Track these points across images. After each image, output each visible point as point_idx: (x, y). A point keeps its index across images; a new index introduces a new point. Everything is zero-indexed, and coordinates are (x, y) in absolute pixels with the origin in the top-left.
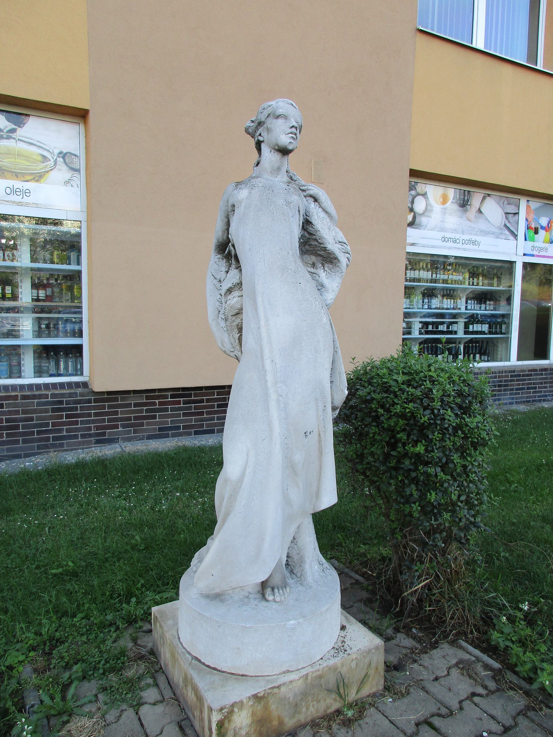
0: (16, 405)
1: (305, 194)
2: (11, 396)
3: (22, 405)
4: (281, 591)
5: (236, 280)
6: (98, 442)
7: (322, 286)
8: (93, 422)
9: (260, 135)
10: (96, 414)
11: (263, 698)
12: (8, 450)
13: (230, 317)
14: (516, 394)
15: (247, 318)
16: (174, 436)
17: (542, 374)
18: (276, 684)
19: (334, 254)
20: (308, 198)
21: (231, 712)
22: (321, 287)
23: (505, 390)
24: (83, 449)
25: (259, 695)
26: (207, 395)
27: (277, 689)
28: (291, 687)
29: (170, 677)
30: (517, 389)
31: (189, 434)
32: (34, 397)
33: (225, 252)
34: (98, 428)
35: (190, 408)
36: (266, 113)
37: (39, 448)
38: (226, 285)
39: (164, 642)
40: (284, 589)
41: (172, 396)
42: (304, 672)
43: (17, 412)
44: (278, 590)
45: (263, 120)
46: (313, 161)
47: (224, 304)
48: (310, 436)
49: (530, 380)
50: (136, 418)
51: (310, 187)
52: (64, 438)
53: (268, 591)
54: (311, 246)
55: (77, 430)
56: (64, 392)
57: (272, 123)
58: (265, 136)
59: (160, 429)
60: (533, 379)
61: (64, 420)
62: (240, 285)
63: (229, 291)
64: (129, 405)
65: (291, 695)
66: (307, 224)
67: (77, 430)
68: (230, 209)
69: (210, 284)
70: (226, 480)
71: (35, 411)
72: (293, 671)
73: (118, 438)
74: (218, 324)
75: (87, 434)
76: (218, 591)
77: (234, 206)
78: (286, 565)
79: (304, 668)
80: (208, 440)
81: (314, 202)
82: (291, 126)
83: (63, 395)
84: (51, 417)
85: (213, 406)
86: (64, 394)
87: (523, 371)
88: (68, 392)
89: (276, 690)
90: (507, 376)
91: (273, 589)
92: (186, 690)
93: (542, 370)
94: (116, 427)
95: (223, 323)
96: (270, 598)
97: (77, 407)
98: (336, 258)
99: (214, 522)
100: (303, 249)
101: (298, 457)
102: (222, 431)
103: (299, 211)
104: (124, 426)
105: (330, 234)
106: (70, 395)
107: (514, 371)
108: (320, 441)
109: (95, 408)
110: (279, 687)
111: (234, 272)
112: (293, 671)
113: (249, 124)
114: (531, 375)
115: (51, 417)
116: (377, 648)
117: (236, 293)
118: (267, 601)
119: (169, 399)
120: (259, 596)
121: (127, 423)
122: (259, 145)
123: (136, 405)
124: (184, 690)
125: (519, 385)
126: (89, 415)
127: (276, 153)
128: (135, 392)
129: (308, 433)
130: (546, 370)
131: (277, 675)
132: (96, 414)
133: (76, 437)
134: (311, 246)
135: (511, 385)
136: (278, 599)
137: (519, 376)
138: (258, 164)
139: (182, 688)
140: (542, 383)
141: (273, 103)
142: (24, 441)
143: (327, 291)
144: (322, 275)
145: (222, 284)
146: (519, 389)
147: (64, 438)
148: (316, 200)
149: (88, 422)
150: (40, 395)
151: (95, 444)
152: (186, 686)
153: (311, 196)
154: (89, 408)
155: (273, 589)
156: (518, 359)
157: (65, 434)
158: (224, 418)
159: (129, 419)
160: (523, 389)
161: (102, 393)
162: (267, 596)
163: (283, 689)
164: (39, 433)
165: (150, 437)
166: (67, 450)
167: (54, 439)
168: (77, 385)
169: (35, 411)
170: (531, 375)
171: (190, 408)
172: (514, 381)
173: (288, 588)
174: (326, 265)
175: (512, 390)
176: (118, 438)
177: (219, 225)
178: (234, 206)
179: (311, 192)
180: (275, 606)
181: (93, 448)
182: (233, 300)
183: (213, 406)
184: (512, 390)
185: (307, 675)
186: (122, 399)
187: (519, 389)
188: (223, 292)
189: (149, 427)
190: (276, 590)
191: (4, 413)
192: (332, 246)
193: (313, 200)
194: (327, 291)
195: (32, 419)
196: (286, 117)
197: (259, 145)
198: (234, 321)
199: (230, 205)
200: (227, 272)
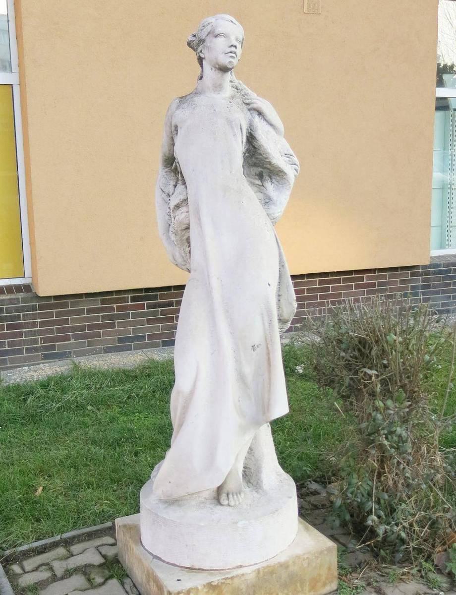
1: (249, 107)
4: (235, 496)
5: (182, 197)
6: (46, 357)
7: (270, 199)
8: (40, 333)
9: (201, 51)
10: (43, 324)
13: (180, 232)
15: (193, 233)
18: (229, 576)
19: (279, 168)
20: (252, 112)
24: (28, 366)
25: (213, 584)
27: (230, 580)
28: (243, 579)
29: (134, 580)
31: (156, 345)
33: (172, 165)
34: (45, 340)
35: (156, 313)
36: (205, 31)
38: (174, 201)
39: (128, 549)
40: (239, 495)
41: (134, 299)
42: (256, 567)
44: (233, 496)
45: (203, 38)
47: (173, 219)
48: (258, 349)
51: (254, 101)
53: (223, 497)
54: (258, 164)
55: (21, 343)
56: (4, 298)
57: (212, 42)
58: (206, 54)
59: (120, 340)
61: (5, 331)
62: (185, 201)
63: (177, 207)
64: (81, 312)
65: (243, 587)
66: (251, 139)
67: (21, 343)
68: (173, 128)
69: (158, 197)
70: (178, 392)
72: (246, 566)
73: (70, 352)
74: (169, 238)
77: (177, 127)
78: (243, 476)
79: (257, 564)
80: (158, 355)
81: (258, 114)
82: (230, 45)
86: (3, 300)
88: (8, 297)
89: (228, 581)
91: (228, 495)
92: (149, 585)
94: (67, 338)
95: (173, 238)
96: (226, 502)
97: (19, 316)
98: (282, 171)
100: (250, 161)
101: (248, 370)
102: (172, 343)
103: (241, 129)
104: (76, 337)
105: (275, 147)
106: (11, 301)
109: (41, 316)
110: (232, 578)
111: (180, 187)
112: (246, 566)
113: (190, 38)
116: (329, 550)
118: (222, 505)
119: (130, 303)
120: (215, 501)
121: (80, 333)
122: (200, 60)
123: (90, 311)
124: (148, 586)
126: (34, 325)
127: (217, 71)
128: (88, 295)
129: (256, 346)
131: (231, 569)
132: (43, 324)
133: (20, 351)
134: (258, 164)
136: (232, 503)
139: (146, 585)
141: (211, 20)
144: (270, 187)
145: (171, 198)
148: (260, 113)
149: (34, 333)
151: (43, 359)
152: (148, 582)
153: (255, 109)
154: (34, 316)
157: (7, 348)
159: (82, 328)
161: (49, 298)
162: (222, 501)
163: (236, 581)
165: (108, 350)
166: (11, 368)
168: (19, 288)
171: (156, 313)
173: (242, 495)
174: (273, 177)
176: (70, 352)
177: (164, 139)
178: (176, 127)
179: (255, 106)
180: (229, 509)
181: (41, 365)
182: (181, 215)
185: (259, 571)
186: (73, 305)
188: (172, 206)
189: (109, 337)
190: (231, 496)
191: (5, 336)
193: (257, 113)
196: (225, 36)
197: (200, 60)
198: (183, 236)
199: (173, 126)
200: (175, 186)
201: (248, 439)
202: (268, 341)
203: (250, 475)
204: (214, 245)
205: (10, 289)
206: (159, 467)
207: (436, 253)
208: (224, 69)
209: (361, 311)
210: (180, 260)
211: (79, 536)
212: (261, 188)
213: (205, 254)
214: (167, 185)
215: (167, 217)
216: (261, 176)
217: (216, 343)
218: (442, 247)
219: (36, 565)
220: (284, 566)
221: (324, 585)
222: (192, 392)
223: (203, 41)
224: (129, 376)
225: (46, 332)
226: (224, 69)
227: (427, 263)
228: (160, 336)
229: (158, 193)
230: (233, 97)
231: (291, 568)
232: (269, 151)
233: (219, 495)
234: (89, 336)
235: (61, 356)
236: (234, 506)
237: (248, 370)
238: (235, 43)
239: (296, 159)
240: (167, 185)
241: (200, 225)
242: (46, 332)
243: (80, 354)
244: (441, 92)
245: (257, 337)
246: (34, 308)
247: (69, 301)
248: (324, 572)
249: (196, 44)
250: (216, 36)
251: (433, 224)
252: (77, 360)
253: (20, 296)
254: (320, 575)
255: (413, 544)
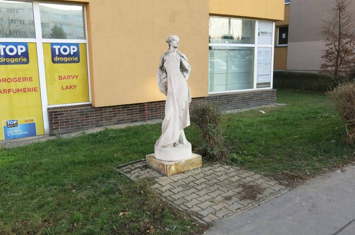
0: (68, 114)
2: (66, 110)
3: (70, 113)
6: (97, 126)
8: (94, 119)
10: (95, 116)
11: (177, 164)
12: (66, 130)
14: (256, 102)
16: (124, 123)
17: (267, 93)
21: (171, 166)
22: (184, 76)
23: (251, 101)
24: (91, 129)
26: (135, 107)
30: (256, 100)
32: (74, 110)
34: (96, 121)
35: (129, 112)
37: (76, 129)
38: (162, 77)
41: (122, 108)
43: (68, 116)
46: (171, 14)
49: (262, 96)
50: (109, 117)
52: (85, 125)
54: (183, 69)
55: (89, 122)
58: (171, 44)
60: (263, 96)
64: (107, 112)
66: (181, 63)
70: (166, 120)
71: (74, 116)
75: (93, 123)
76: (164, 146)
83: (83, 109)
84: (80, 118)
85: (137, 111)
87: (258, 92)
90: (252, 95)
91: (177, 145)
93: (267, 92)
95: (161, 85)
97: (88, 113)
98: (188, 70)
99: (161, 133)
104: (105, 120)
105: (186, 64)
106: (86, 109)
107: (255, 93)
108: (186, 111)
109: (95, 113)
110: (180, 162)
113: (167, 40)
114: (262, 94)
115: (80, 118)
117: (165, 79)
122: (170, 45)
123: (109, 112)
125: (257, 98)
126: (93, 116)
130: (268, 91)
132: (95, 116)
133: (89, 125)
134: (183, 69)
135: (254, 98)
136: (178, 146)
137: (257, 94)
138: (169, 49)
140: (267, 97)
141: (172, 36)
142: (71, 127)
143: (186, 77)
144: (185, 73)
146: (257, 100)
147: (85, 125)
148: (183, 57)
150: (76, 109)
154: (93, 114)
155: (177, 145)
156: (257, 87)
158: (164, 108)
160: (259, 100)
161: (97, 108)
163: (181, 163)
164: (76, 123)
165: (115, 124)
167: (82, 125)
168: (88, 105)
169: (74, 116)
170: (262, 94)
172: (255, 96)
175: (255, 100)
183: (137, 111)
184: (255, 100)
185: (185, 161)
187: (257, 100)
189: (115, 120)
192: (187, 67)
194: (186, 77)
195: (73, 118)
196: (176, 40)
197: (170, 45)
201: (180, 133)
202: (186, 108)
203: (180, 141)
204: (173, 87)
205: (86, 105)
206: (158, 142)
207: (210, 93)
208: (175, 48)
209: (200, 104)
210: (163, 91)
211: (133, 163)
212: (183, 73)
213: (172, 89)
214: (160, 73)
215: (160, 81)
216: (182, 71)
217: (175, 108)
218: (211, 91)
219: (126, 168)
220: (191, 160)
221: (199, 165)
222: (170, 120)
223: (171, 41)
224: (123, 130)
225: (97, 118)
226: (175, 48)
227: (208, 96)
228: (130, 119)
229: (158, 75)
230: (177, 53)
231: (192, 161)
232: (185, 65)
233: (175, 145)
234: (109, 119)
235: (100, 126)
236: (179, 147)
237: (182, 115)
238: (178, 42)
239: (190, 67)
240: (160, 73)
241: (171, 82)
242: (97, 118)
243: (107, 125)
244: (210, 45)
245: (184, 107)
246: (93, 111)
247: (103, 109)
248: (199, 162)
249: (169, 42)
250: (174, 40)
251: (209, 85)
252: (106, 127)
253: (89, 107)
254: (198, 163)
255: (218, 157)
